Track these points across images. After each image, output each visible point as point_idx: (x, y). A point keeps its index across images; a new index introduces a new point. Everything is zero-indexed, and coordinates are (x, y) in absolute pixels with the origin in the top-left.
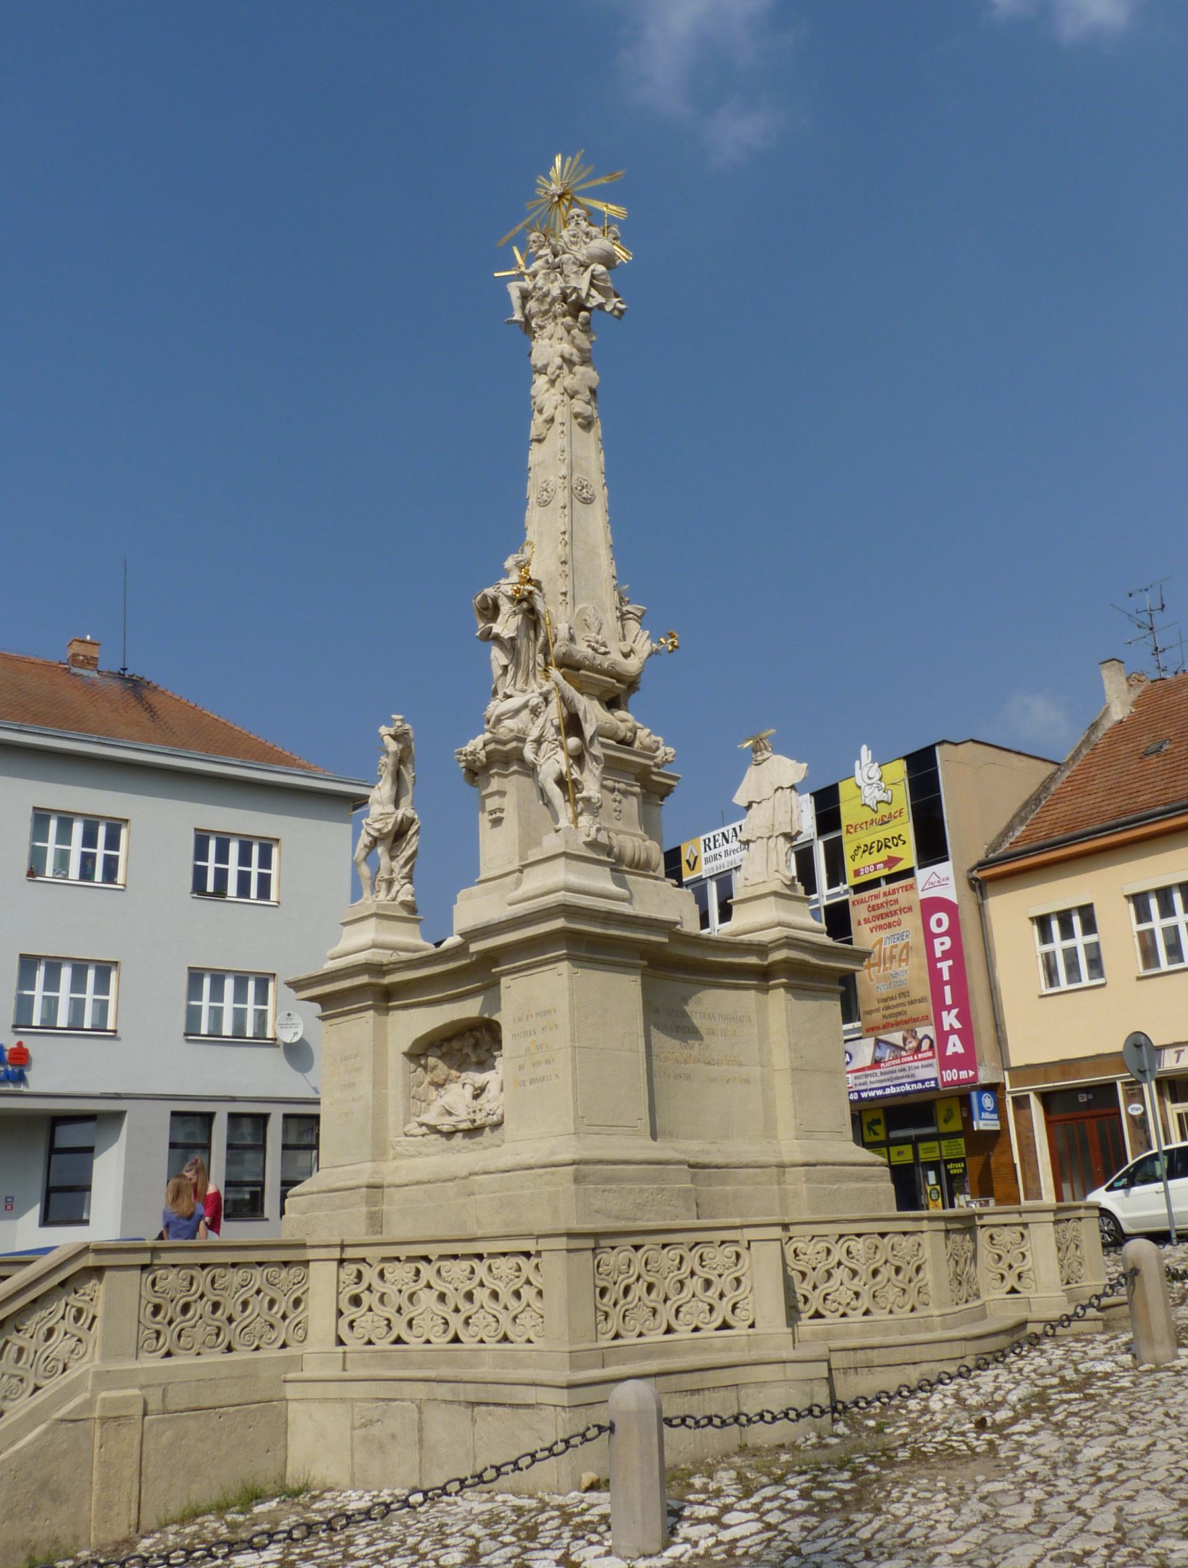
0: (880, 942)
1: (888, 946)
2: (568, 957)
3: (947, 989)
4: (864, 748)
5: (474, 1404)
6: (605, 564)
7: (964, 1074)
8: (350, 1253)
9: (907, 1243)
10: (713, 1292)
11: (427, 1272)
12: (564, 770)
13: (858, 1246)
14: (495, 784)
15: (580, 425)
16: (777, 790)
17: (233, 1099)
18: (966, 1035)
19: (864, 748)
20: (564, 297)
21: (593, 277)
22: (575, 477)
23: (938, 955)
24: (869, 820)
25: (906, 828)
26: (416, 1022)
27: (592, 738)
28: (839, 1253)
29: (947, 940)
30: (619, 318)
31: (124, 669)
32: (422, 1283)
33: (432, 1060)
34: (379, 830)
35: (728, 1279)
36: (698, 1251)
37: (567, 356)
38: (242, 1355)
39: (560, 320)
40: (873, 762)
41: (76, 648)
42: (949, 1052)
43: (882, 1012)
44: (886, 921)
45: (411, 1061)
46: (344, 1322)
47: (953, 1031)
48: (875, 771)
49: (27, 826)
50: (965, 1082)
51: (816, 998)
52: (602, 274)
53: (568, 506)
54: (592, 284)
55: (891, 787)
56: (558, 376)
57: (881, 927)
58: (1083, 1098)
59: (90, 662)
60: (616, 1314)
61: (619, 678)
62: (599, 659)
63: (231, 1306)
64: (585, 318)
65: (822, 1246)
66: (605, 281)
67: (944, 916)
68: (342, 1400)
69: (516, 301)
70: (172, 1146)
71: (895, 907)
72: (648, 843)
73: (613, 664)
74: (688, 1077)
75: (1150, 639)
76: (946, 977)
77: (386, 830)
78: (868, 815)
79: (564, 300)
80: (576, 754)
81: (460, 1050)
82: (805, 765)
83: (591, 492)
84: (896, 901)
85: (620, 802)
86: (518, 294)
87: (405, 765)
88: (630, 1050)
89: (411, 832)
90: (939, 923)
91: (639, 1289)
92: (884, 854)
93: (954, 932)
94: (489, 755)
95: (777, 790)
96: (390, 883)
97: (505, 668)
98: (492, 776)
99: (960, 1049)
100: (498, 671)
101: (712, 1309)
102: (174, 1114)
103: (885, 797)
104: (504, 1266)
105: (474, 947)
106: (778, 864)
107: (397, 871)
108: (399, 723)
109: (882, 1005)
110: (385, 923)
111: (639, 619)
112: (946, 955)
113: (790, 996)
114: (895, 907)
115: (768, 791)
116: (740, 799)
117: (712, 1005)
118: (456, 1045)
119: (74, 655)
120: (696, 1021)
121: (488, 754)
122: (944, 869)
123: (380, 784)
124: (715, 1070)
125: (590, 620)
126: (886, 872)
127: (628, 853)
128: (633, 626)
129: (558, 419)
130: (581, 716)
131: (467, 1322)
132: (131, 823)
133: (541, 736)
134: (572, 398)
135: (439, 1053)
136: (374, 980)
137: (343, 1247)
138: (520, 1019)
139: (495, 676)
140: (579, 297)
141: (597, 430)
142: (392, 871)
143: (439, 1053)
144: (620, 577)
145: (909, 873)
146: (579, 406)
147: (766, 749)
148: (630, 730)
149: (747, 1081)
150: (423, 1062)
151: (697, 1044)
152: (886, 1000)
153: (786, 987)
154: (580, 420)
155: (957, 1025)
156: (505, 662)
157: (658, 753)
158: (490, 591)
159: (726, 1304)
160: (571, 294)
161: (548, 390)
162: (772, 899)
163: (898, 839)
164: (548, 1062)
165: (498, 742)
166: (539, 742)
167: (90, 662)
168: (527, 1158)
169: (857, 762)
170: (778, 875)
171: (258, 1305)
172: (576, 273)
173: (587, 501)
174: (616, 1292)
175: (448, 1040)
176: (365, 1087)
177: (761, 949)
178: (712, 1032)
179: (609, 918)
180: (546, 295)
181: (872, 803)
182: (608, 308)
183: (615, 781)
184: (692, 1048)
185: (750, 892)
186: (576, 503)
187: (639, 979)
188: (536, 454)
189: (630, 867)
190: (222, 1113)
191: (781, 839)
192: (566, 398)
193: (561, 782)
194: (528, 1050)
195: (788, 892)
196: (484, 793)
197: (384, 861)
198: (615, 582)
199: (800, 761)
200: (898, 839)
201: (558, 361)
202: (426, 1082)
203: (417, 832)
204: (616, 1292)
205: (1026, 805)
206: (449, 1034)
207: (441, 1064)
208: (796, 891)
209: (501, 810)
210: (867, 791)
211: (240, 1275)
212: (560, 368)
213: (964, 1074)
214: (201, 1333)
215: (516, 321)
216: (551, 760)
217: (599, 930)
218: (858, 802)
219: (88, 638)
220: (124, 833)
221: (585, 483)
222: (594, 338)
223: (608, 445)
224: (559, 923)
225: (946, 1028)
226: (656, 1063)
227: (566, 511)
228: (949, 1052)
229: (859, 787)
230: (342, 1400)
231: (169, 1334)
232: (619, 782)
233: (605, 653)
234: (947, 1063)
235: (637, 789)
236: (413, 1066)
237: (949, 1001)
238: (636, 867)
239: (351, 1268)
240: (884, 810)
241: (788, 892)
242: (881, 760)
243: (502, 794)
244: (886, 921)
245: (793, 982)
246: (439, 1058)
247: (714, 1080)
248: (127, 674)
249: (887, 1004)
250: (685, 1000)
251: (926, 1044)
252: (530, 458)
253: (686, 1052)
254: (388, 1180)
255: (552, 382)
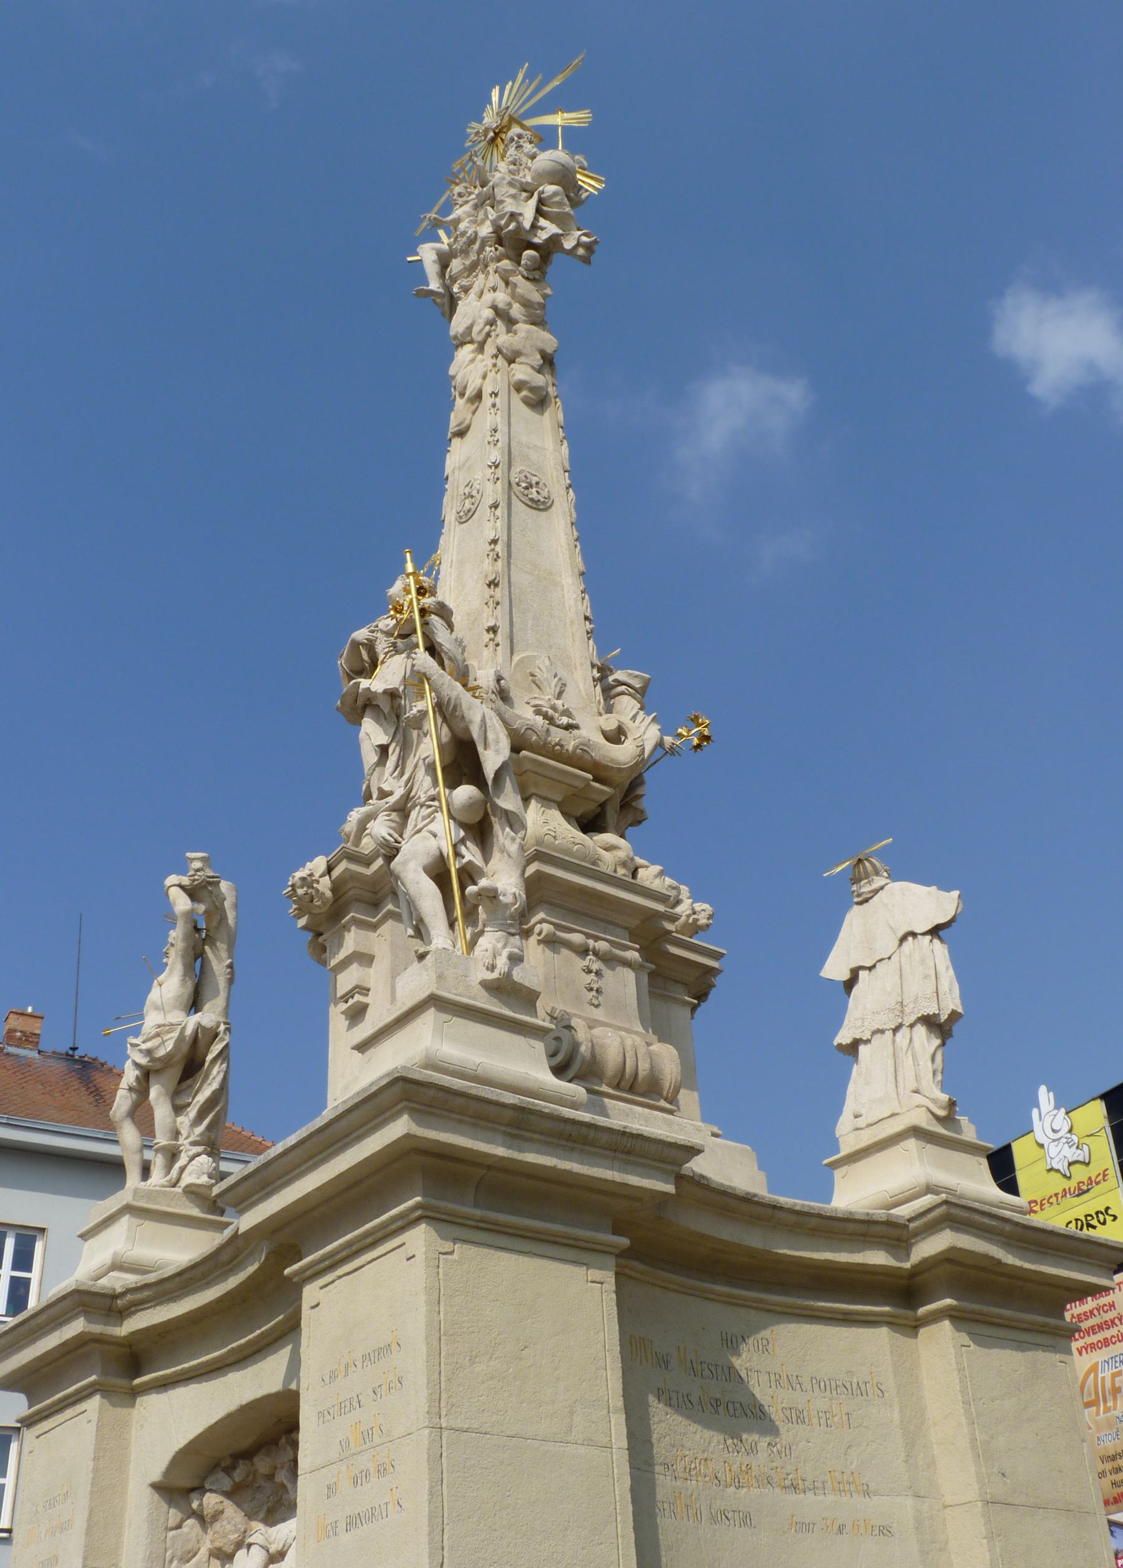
0: (1094, 1369)
1: (1108, 1374)
4: (1043, 1090)
6: (570, 599)
12: (448, 850)
14: (352, 940)
15: (526, 401)
16: (903, 939)
19: (1043, 1090)
21: (541, 202)
22: (517, 468)
24: (1060, 1191)
26: (179, 1415)
27: (498, 774)
30: (586, 260)
31: (74, 1049)
33: (211, 1501)
34: (149, 1052)
37: (501, 305)
40: (1057, 1107)
41: (14, 1022)
43: (1110, 1478)
44: (1100, 1336)
45: (171, 1502)
48: (1061, 1120)
51: (1021, 1346)
52: (555, 194)
53: (503, 506)
54: (539, 212)
55: (1086, 1140)
56: (488, 335)
57: (1093, 1347)
59: (29, 1039)
61: (600, 772)
62: (557, 735)
64: (531, 258)
66: (560, 204)
69: (431, 268)
71: (1111, 1315)
72: (657, 1047)
73: (585, 747)
74: (746, 1520)
77: (161, 1053)
78: (1057, 1184)
79: (500, 241)
80: (476, 818)
81: (270, 1477)
82: (955, 894)
83: (545, 493)
84: (1112, 1306)
85: (598, 973)
86: (434, 257)
87: (213, 945)
88: (589, 1443)
89: (209, 1057)
94: (337, 887)
95: (903, 939)
96: (172, 1155)
97: (383, 750)
98: (346, 928)
100: (370, 757)
103: (1079, 1155)
106: (917, 1078)
107: (184, 1132)
108: (197, 865)
109: (1108, 1466)
110: (149, 1226)
111: (641, 693)
113: (964, 1338)
114: (1111, 1315)
115: (886, 944)
116: (835, 969)
117: (794, 1357)
119: (11, 1031)
120: (761, 1391)
123: (161, 978)
124: (809, 1505)
125: (542, 675)
127: (611, 1058)
128: (627, 705)
129: (487, 390)
130: (476, 734)
132: (50, 1234)
133: (407, 797)
134: (511, 361)
135: (227, 1483)
136: (97, 1329)
138: (333, 1376)
139: (366, 767)
140: (519, 227)
141: (554, 414)
142: (176, 1134)
143: (227, 1483)
144: (600, 627)
146: (521, 372)
147: (877, 873)
148: (624, 864)
149: (884, 1531)
150: (195, 1505)
151: (763, 1443)
152: (1113, 1458)
153: (957, 1317)
154: (524, 393)
156: (384, 739)
157: (679, 910)
158: (361, 634)
160: (507, 224)
161: (473, 361)
162: (911, 1143)
164: (382, 1471)
165: (353, 858)
167: (29, 1039)
169: (1035, 1112)
170: (919, 1099)
172: (514, 196)
173: (541, 505)
175: (247, 1455)
177: (892, 1233)
178: (798, 1417)
180: (472, 241)
181: (1062, 1166)
182: (568, 244)
183: (589, 936)
184: (752, 1450)
185: (866, 1138)
186: (518, 507)
187: (609, 1278)
188: (457, 454)
189: (617, 1087)
191: (921, 1030)
192: (501, 361)
193: (439, 873)
194: (345, 1444)
195: (940, 1130)
196: (333, 962)
197: (162, 1111)
198: (589, 626)
199: (946, 887)
201: (489, 313)
202: (203, 1552)
203: (223, 1054)
206: (246, 1443)
207: (230, 1509)
208: (959, 1130)
209: (365, 991)
210: (1053, 1150)
212: (492, 323)
215: (432, 292)
216: (424, 833)
217: (501, 1151)
218: (1042, 1167)
219: (30, 1010)
220: (39, 1246)
221: (534, 480)
222: (548, 291)
223: (571, 431)
226: (665, 1485)
227: (498, 512)
229: (1041, 1146)
232: (597, 939)
233: (568, 727)
235: (633, 955)
236: (174, 1515)
238: (631, 1089)
240: (1080, 1174)
241: (940, 1130)
242: (1069, 1104)
243: (365, 959)
244: (1100, 1336)
245: (966, 1305)
246: (228, 1495)
247: (806, 1527)
248: (77, 1054)
249: (1115, 1464)
250: (733, 1343)
252: (448, 463)
253: (738, 1460)
255: (481, 348)
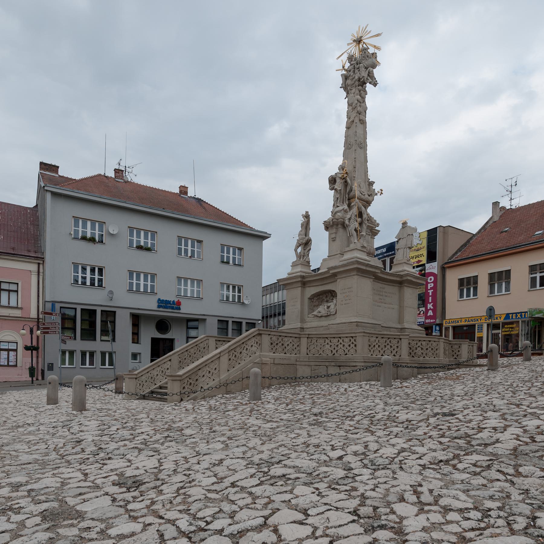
2: (357, 275)
3: (430, 298)
5: (340, 366)
7: (432, 321)
8: (310, 336)
9: (434, 344)
10: (392, 349)
11: (327, 341)
13: (424, 343)
17: (233, 318)
18: (434, 311)
20: (359, 80)
23: (429, 288)
25: (424, 252)
28: (419, 344)
29: (432, 284)
32: (326, 343)
35: (395, 346)
36: (389, 340)
38: (288, 355)
39: (357, 87)
42: (428, 315)
46: (308, 350)
47: (430, 309)
49: (176, 241)
50: (432, 323)
54: (368, 75)
58: (465, 328)
60: (372, 351)
63: (286, 345)
65: (415, 342)
67: (432, 278)
68: (309, 365)
70: (218, 328)
75: (510, 195)
76: (430, 294)
79: (359, 81)
90: (431, 279)
91: (377, 346)
92: (417, 259)
93: (435, 282)
99: (432, 314)
101: (392, 352)
102: (218, 320)
104: (347, 340)
105: (331, 272)
112: (431, 289)
115: (405, 235)
118: (321, 297)
121: (333, 222)
122: (435, 264)
126: (417, 264)
131: (337, 351)
137: (309, 334)
145: (424, 265)
155: (432, 308)
159: (395, 351)
163: (422, 255)
166: (350, 219)
168: (344, 321)
171: (291, 345)
174: (372, 346)
175: (319, 295)
176: (298, 306)
179: (367, 265)
190: (230, 321)
193: (356, 230)
200: (422, 255)
204: (372, 346)
205: (462, 246)
211: (288, 338)
213: (432, 321)
214: (280, 349)
224: (356, 266)
225: (429, 308)
228: (428, 315)
230: (309, 365)
231: (274, 349)
234: (427, 317)
237: (430, 301)
239: (310, 340)
240: (419, 246)
251: (422, 313)
254: (305, 327)
